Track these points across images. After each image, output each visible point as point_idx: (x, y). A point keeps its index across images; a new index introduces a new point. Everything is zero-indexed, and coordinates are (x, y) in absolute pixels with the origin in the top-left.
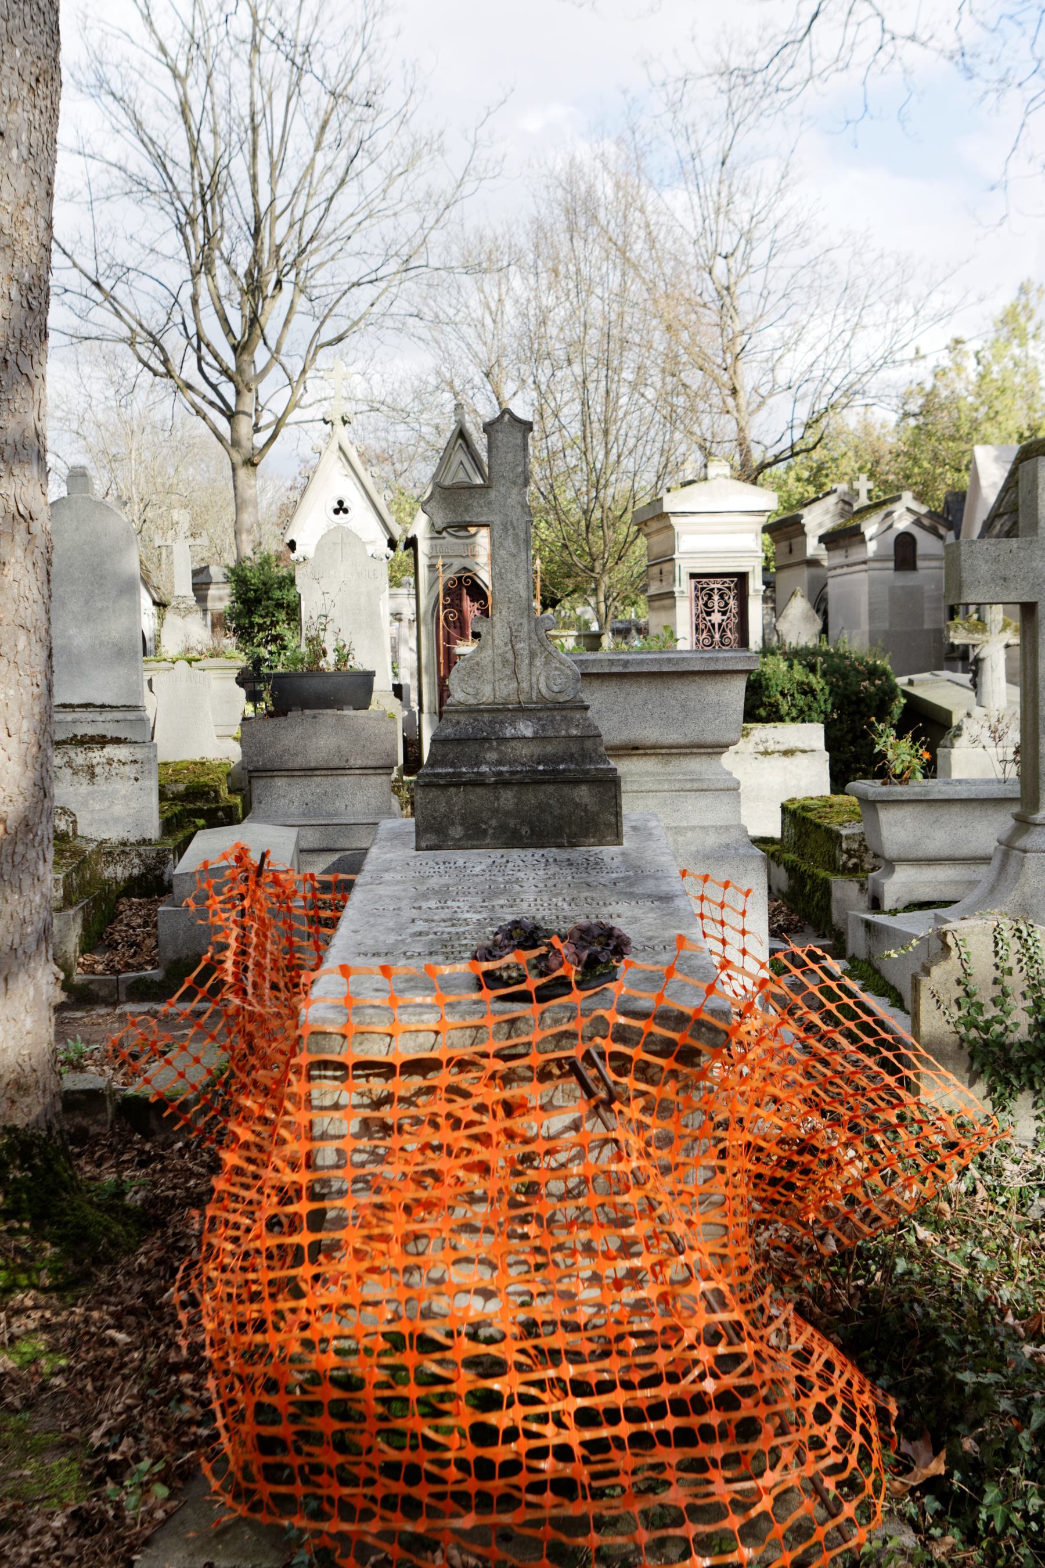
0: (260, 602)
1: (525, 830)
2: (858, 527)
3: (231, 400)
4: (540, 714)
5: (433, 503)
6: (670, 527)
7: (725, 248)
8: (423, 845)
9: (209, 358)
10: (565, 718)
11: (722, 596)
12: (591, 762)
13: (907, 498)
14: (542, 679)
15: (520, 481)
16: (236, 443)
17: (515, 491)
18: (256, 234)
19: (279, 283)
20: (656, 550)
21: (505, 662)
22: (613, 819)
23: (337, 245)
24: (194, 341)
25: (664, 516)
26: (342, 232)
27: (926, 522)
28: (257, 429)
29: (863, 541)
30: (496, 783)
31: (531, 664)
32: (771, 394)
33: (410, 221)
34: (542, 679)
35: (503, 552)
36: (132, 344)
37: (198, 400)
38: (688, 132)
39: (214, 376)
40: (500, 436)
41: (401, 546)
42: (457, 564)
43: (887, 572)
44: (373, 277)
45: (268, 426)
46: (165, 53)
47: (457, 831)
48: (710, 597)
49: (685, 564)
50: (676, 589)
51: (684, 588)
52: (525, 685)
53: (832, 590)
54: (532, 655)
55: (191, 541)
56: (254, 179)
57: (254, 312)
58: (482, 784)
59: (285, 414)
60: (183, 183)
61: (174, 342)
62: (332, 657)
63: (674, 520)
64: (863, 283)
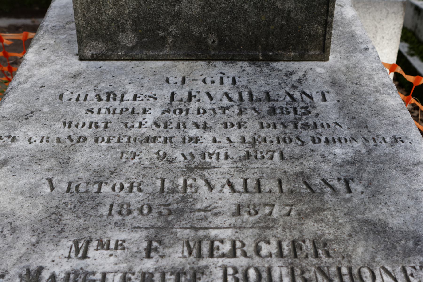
1: (212, 39)
8: (88, 53)
22: (320, 29)
47: (129, 39)
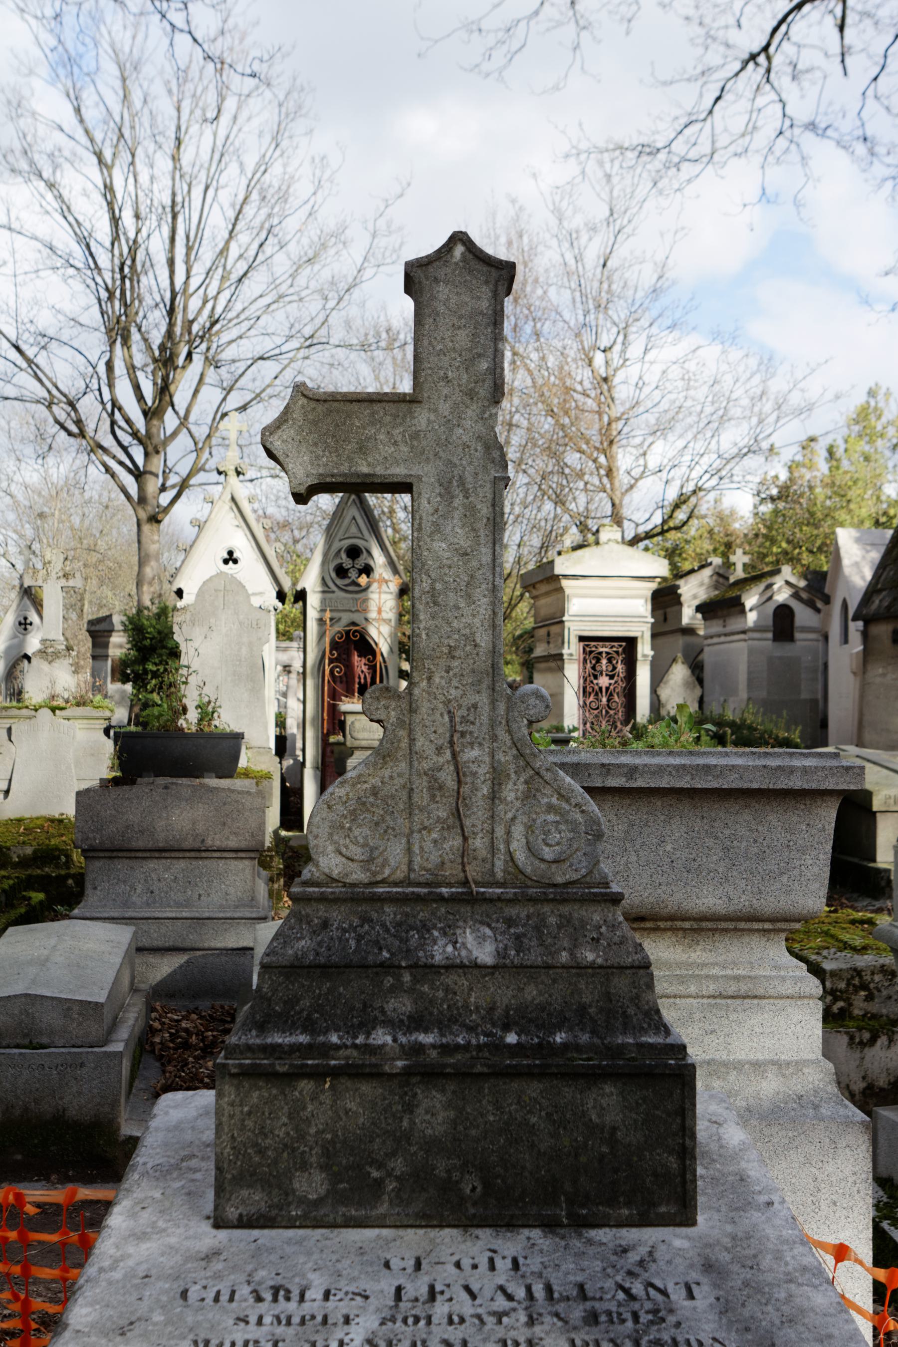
0: (150, 652)
1: (470, 1184)
2: (739, 598)
3: (140, 460)
4: (512, 911)
5: (288, 432)
6: (561, 590)
7: (604, 342)
8: (232, 1213)
9: (122, 423)
10: (566, 922)
11: (610, 660)
12: (627, 1026)
13: (787, 572)
14: (518, 831)
15: (484, 391)
16: (142, 500)
17: (471, 412)
18: (171, 312)
19: (189, 355)
20: (543, 612)
21: (436, 788)
22: (673, 1163)
23: (245, 325)
24: (109, 407)
25: (556, 578)
26: (252, 311)
27: (804, 595)
28: (163, 489)
29: (742, 611)
30: (407, 1073)
31: (494, 797)
32: (641, 477)
33: (314, 306)
34: (518, 831)
35: (440, 546)
36: (49, 407)
37: (112, 464)
38: (572, 239)
39: (126, 439)
40: (443, 291)
41: (290, 598)
42: (346, 618)
43: (766, 642)
44: (277, 351)
45: (173, 486)
46: (92, 140)
47: (311, 1184)
48: (598, 660)
49: (574, 627)
50: (565, 651)
51: (572, 650)
52: (479, 843)
53: (707, 657)
54: (498, 777)
55: (63, 582)
56: (171, 263)
57: (165, 379)
58: (375, 1074)
59: (190, 475)
60: (104, 260)
61: (89, 408)
62: (193, 715)
63: (565, 583)
64: (728, 380)
